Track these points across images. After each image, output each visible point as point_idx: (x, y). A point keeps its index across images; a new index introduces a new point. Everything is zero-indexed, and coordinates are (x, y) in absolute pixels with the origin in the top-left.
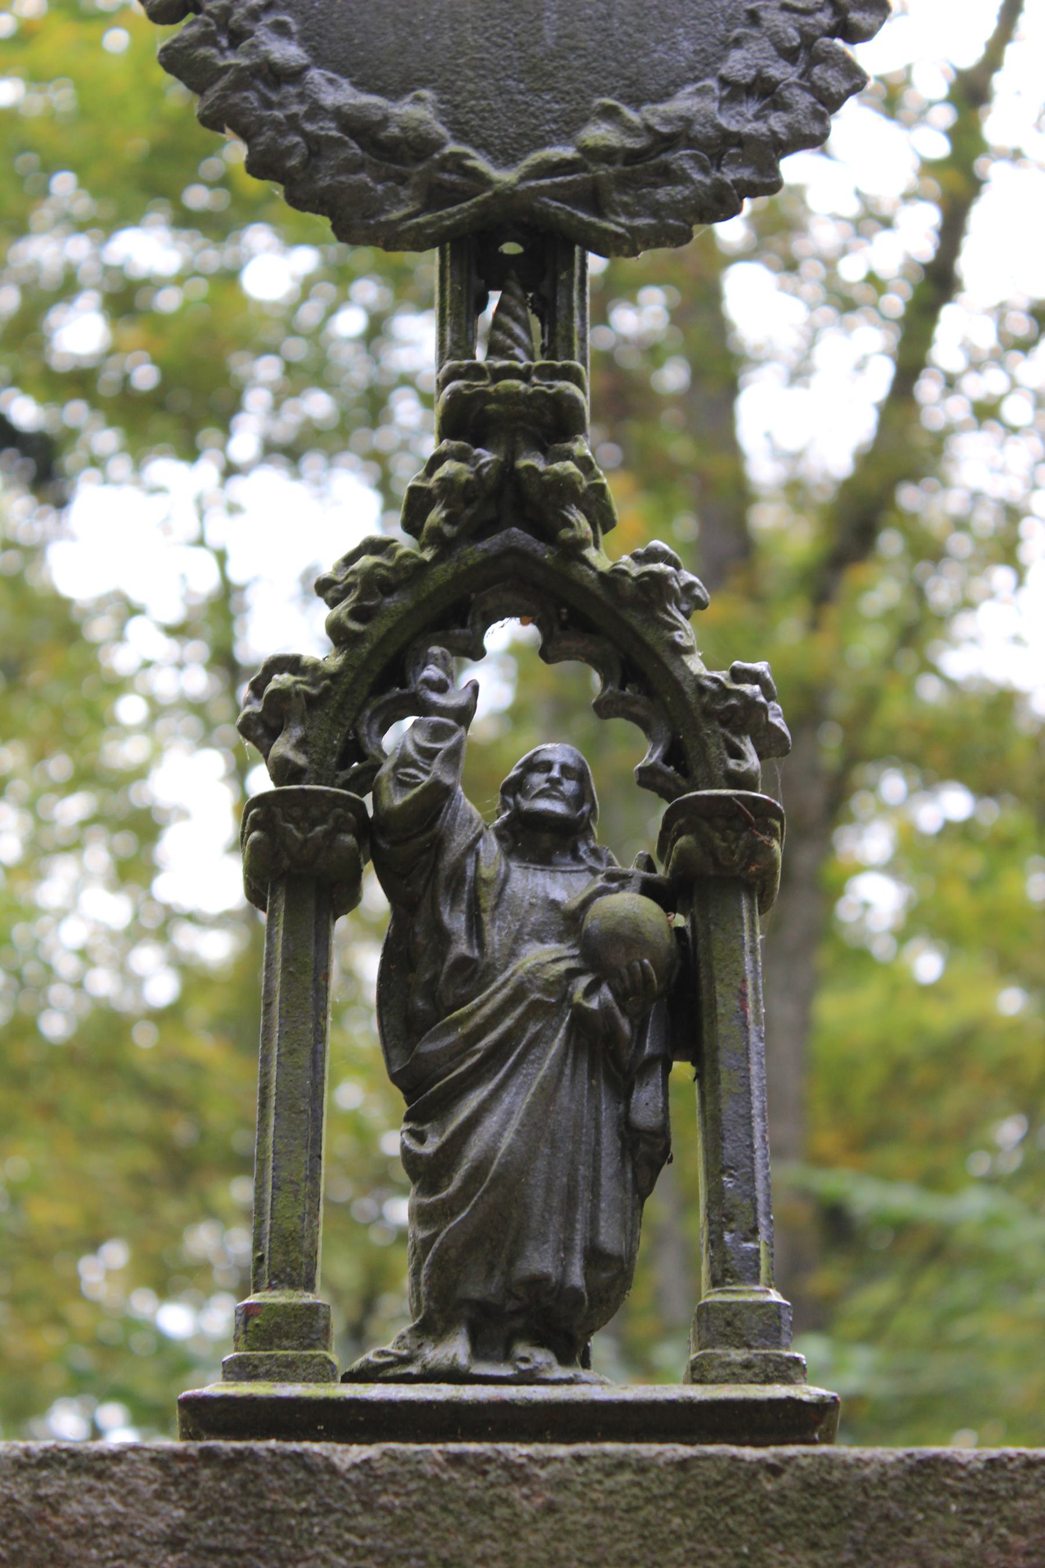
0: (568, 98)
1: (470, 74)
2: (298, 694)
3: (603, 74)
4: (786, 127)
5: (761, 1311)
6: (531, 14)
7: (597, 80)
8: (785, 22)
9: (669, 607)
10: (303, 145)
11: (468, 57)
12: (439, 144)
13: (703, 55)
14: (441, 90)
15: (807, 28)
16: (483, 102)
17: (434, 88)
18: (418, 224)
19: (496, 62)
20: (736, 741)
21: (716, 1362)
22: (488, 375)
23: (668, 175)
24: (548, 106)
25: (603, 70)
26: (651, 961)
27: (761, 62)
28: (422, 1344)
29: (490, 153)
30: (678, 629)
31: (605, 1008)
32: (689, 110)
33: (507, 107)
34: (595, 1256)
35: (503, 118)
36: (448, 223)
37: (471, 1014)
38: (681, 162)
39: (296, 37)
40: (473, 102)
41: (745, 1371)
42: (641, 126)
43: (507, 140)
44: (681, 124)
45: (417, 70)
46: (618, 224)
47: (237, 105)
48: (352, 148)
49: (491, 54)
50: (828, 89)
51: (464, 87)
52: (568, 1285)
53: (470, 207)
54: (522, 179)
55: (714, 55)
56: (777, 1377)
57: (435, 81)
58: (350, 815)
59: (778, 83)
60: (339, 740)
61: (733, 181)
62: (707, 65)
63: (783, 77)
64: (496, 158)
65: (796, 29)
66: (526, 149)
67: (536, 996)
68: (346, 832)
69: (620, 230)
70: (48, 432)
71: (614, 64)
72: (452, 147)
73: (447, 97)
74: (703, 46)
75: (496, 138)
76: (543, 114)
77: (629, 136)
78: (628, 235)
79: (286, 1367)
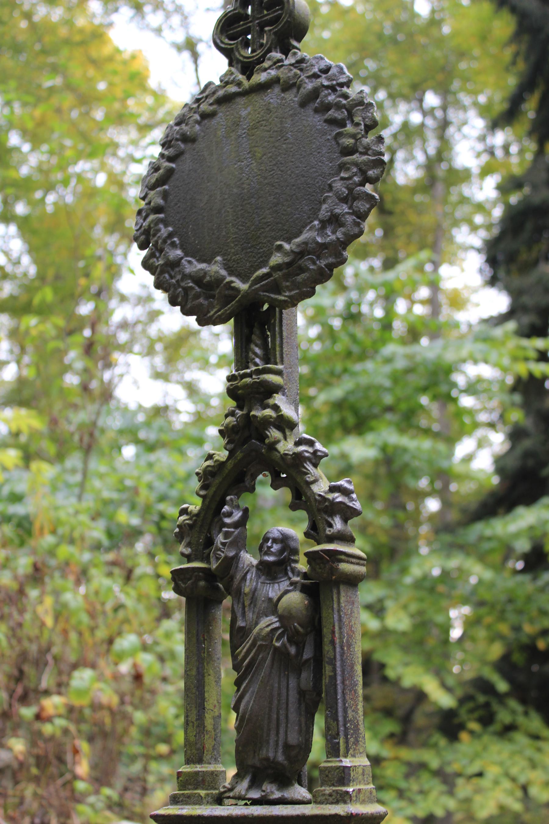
0: (265, 245)
1: (232, 245)
2: (185, 525)
3: (277, 231)
4: (343, 234)
5: (338, 771)
6: (250, 212)
7: (275, 234)
8: (341, 186)
9: (305, 465)
10: (182, 292)
11: (231, 238)
12: (224, 278)
13: (313, 210)
14: (223, 255)
15: (350, 186)
17: (221, 255)
18: (219, 315)
19: (240, 237)
20: (330, 519)
21: (320, 794)
22: (239, 378)
23: (302, 270)
24: (259, 251)
25: (277, 229)
26: (299, 624)
27: (332, 208)
28: (237, 782)
29: (241, 277)
30: (308, 474)
31: (283, 645)
32: (306, 238)
33: (245, 256)
34: (287, 747)
35: (244, 261)
36: (228, 312)
37: (241, 651)
38: (305, 263)
39: (179, 246)
40: (234, 257)
41: (330, 798)
42: (289, 251)
44: (303, 246)
45: (216, 249)
46: (285, 296)
47: (162, 280)
48: (196, 289)
49: (238, 234)
51: (230, 251)
52: (276, 760)
53: (235, 303)
54: (250, 287)
55: (317, 209)
56: (341, 800)
57: (221, 251)
58: (201, 574)
59: (339, 215)
60: (202, 539)
61: (325, 265)
62: (314, 214)
63: (341, 211)
64: (243, 279)
65: (345, 188)
66: (253, 272)
67: (259, 643)
68: (200, 580)
69: (286, 298)
70: (485, 252)
72: (228, 279)
73: (226, 257)
75: (243, 270)
76: (257, 255)
78: (289, 300)
79: (188, 798)
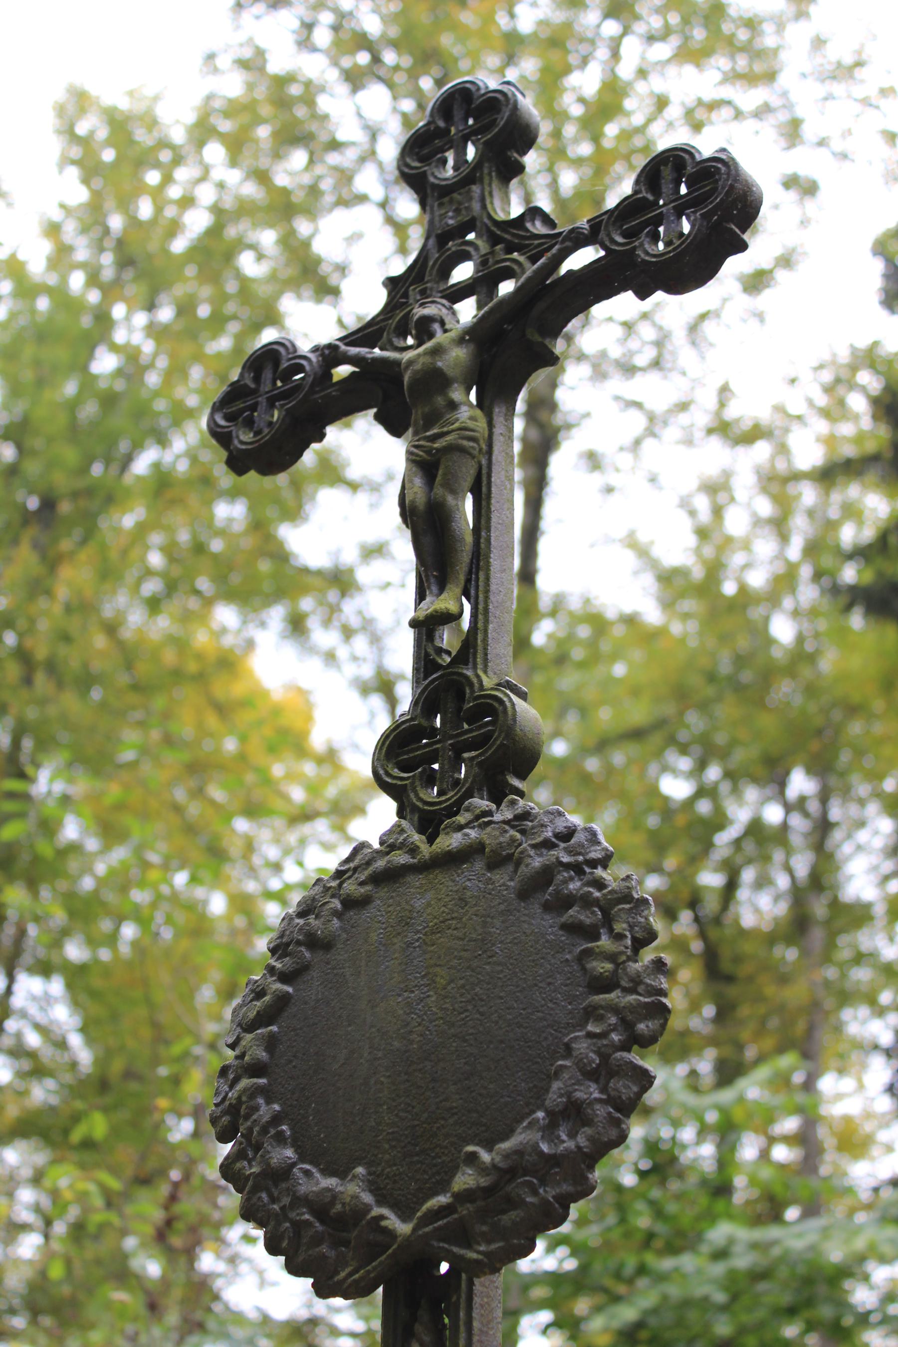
4: (588, 1140)
8: (587, 1048)
12: (368, 1208)
15: (603, 1049)
16: (394, 1168)
18: (355, 1281)
27: (570, 1089)
36: (372, 1275)
38: (517, 1190)
40: (388, 1170)
43: (410, 1196)
50: (620, 1097)
53: (386, 1259)
65: (595, 1052)
71: (475, 1115)
72: (377, 1211)
74: (535, 1083)
77: (482, 1177)
